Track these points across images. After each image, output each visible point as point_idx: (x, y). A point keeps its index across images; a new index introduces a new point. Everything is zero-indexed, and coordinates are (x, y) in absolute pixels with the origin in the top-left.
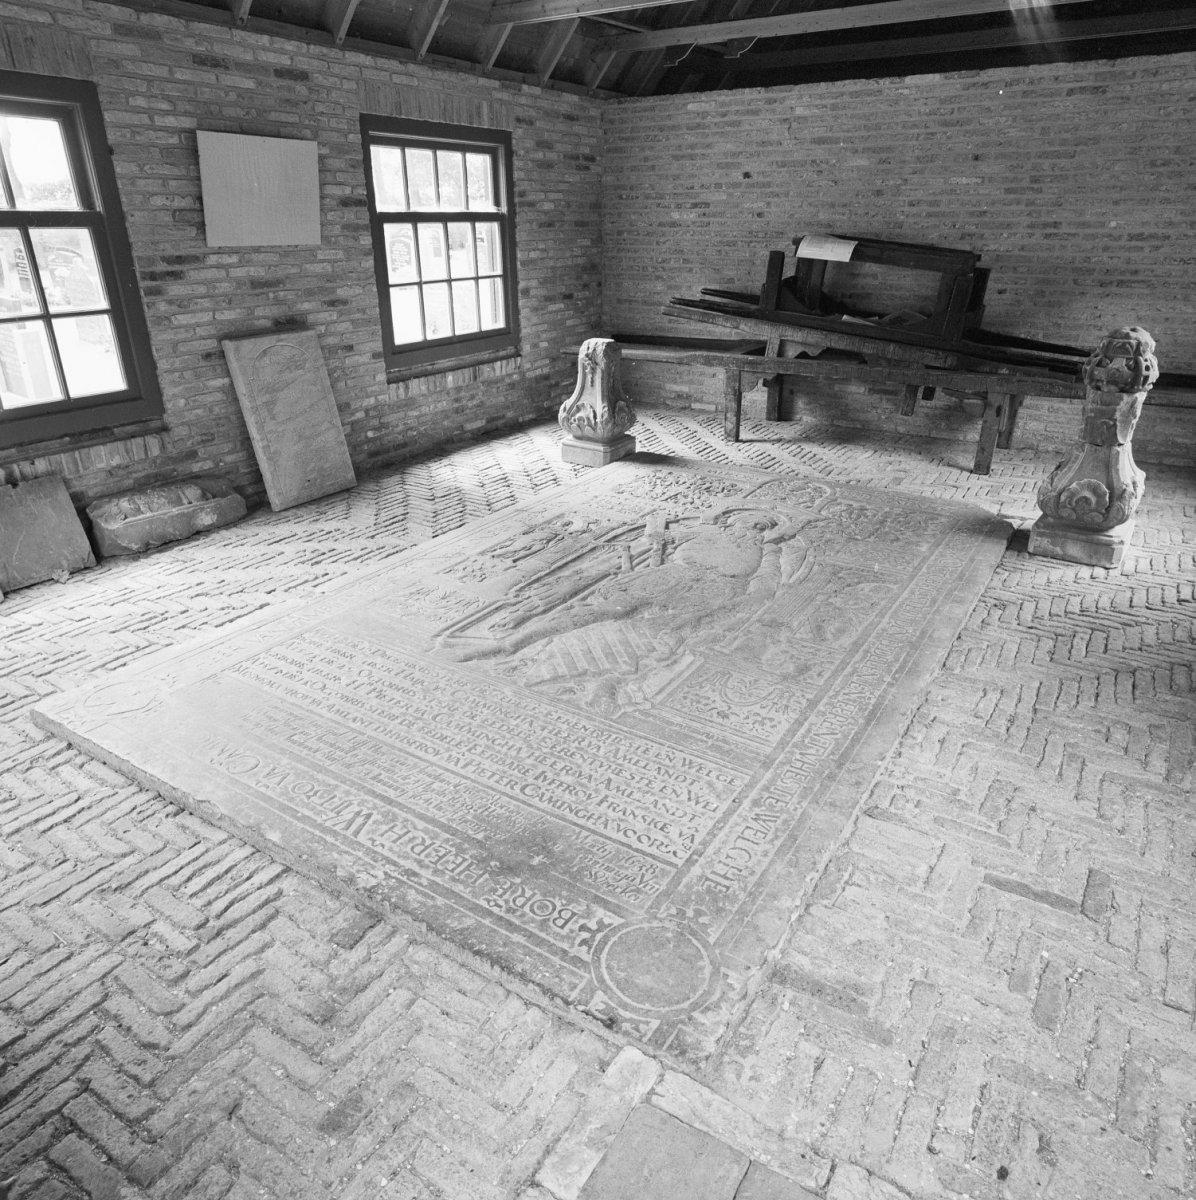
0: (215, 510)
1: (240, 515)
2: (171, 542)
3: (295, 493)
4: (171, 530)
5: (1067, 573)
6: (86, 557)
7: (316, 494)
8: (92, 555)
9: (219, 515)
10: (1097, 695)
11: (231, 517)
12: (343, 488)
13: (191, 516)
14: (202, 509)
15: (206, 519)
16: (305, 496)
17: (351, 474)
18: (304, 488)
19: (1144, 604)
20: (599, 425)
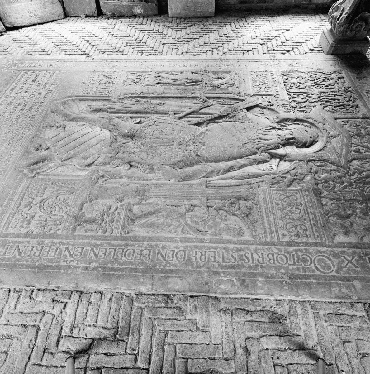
0: (142, 8)
1: (154, 14)
2: (124, 16)
3: (179, 11)
4: (123, 11)
5: (192, 168)
6: (94, 12)
7: (190, 14)
8: (96, 11)
9: (145, 11)
10: (22, 313)
11: (151, 13)
12: (205, 15)
13: (131, 8)
14: (137, 6)
15: (138, 11)
16: (183, 14)
17: (212, 9)
18: (184, 9)
19: (271, 21)
20: (223, 270)
